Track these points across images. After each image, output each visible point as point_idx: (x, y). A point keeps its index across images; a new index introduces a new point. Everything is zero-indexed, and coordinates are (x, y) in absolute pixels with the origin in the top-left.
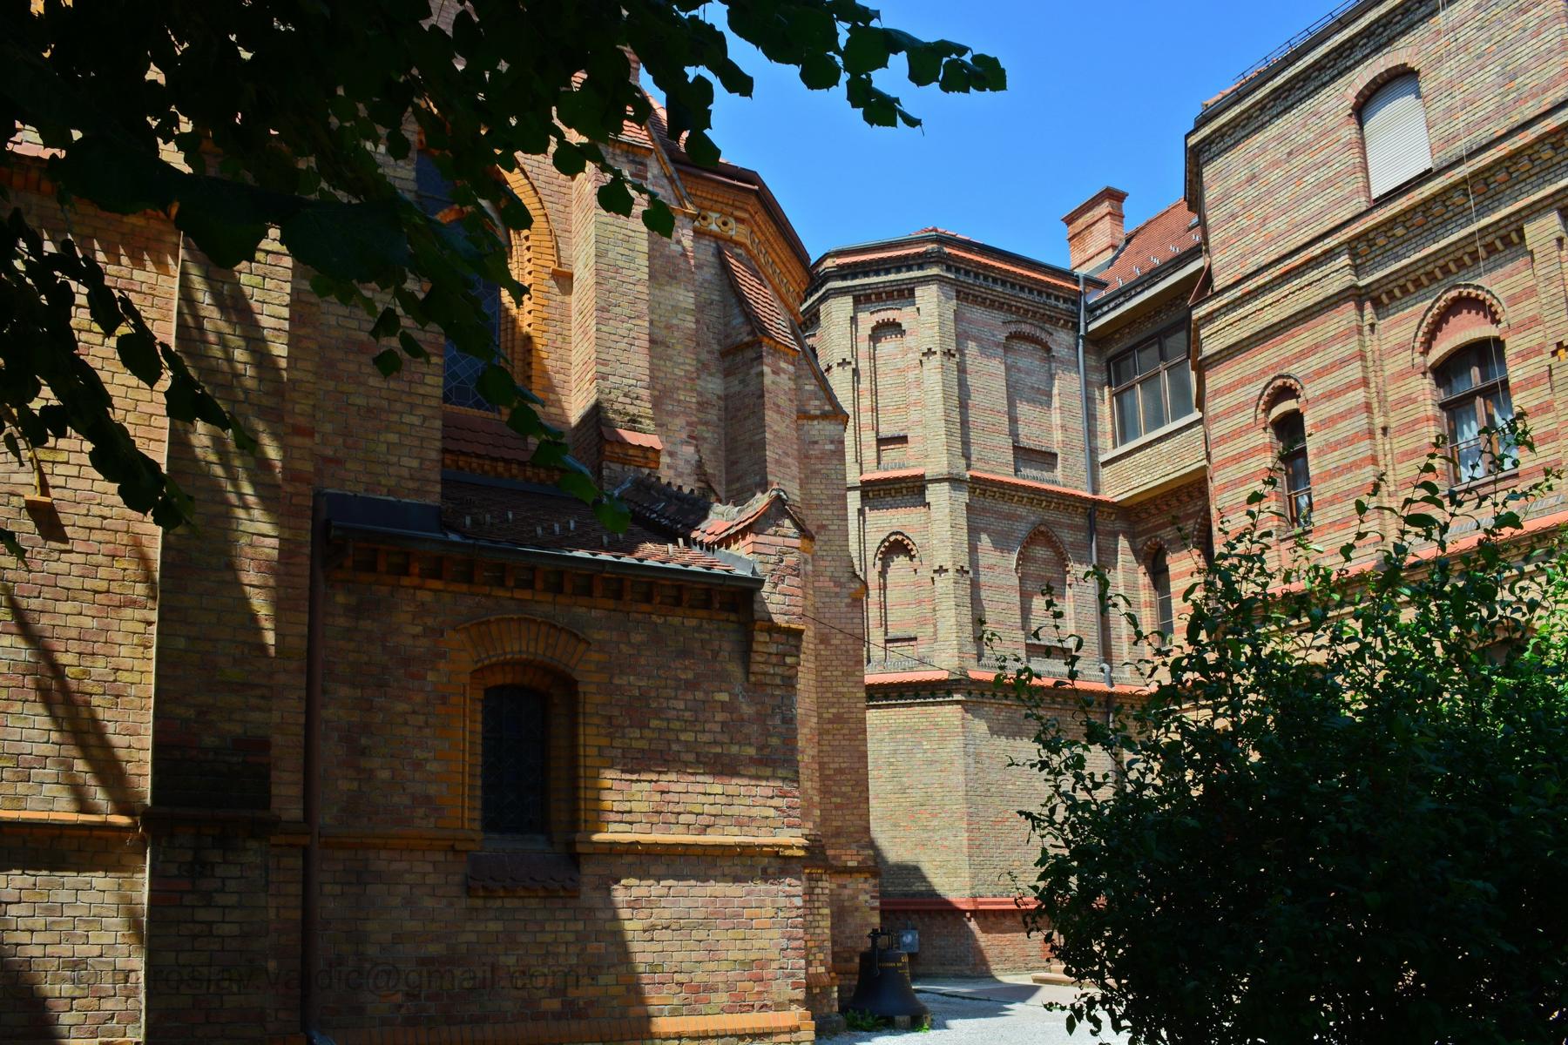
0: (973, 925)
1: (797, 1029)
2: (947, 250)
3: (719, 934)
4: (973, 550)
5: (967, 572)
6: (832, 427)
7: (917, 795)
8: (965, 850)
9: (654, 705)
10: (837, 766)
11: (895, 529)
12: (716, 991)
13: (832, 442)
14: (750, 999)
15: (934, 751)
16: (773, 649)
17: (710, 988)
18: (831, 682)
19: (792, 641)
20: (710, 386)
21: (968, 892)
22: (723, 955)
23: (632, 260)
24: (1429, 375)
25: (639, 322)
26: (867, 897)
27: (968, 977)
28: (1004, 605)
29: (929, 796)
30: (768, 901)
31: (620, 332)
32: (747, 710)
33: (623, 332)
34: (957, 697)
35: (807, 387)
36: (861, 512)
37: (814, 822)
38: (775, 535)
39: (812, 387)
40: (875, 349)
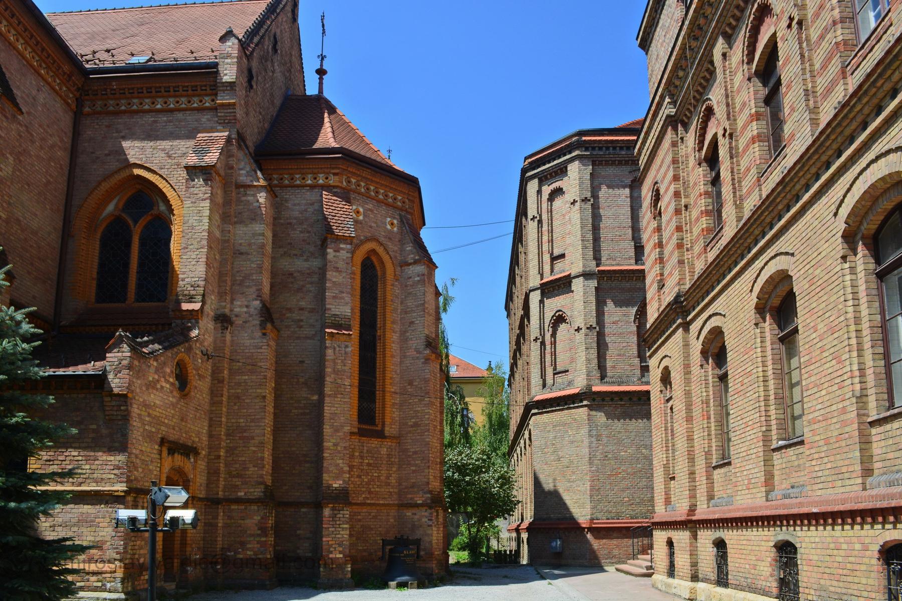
0: (589, 536)
1: (115, 572)
2: (584, 138)
3: (84, 530)
4: (600, 314)
5: (595, 328)
6: (418, 268)
7: (565, 461)
8: (588, 492)
10: (413, 450)
11: (559, 309)
13: (418, 276)
15: (574, 435)
16: (114, 403)
19: (122, 399)
21: (589, 517)
23: (201, 221)
24: (704, 164)
25: (202, 250)
26: (426, 520)
27: (586, 567)
28: (624, 344)
29: (571, 462)
30: (107, 515)
31: (192, 257)
32: (104, 431)
33: (194, 257)
34: (585, 403)
35: (408, 249)
36: (542, 302)
37: (344, 481)
38: (118, 352)
39: (410, 248)
40: (551, 205)
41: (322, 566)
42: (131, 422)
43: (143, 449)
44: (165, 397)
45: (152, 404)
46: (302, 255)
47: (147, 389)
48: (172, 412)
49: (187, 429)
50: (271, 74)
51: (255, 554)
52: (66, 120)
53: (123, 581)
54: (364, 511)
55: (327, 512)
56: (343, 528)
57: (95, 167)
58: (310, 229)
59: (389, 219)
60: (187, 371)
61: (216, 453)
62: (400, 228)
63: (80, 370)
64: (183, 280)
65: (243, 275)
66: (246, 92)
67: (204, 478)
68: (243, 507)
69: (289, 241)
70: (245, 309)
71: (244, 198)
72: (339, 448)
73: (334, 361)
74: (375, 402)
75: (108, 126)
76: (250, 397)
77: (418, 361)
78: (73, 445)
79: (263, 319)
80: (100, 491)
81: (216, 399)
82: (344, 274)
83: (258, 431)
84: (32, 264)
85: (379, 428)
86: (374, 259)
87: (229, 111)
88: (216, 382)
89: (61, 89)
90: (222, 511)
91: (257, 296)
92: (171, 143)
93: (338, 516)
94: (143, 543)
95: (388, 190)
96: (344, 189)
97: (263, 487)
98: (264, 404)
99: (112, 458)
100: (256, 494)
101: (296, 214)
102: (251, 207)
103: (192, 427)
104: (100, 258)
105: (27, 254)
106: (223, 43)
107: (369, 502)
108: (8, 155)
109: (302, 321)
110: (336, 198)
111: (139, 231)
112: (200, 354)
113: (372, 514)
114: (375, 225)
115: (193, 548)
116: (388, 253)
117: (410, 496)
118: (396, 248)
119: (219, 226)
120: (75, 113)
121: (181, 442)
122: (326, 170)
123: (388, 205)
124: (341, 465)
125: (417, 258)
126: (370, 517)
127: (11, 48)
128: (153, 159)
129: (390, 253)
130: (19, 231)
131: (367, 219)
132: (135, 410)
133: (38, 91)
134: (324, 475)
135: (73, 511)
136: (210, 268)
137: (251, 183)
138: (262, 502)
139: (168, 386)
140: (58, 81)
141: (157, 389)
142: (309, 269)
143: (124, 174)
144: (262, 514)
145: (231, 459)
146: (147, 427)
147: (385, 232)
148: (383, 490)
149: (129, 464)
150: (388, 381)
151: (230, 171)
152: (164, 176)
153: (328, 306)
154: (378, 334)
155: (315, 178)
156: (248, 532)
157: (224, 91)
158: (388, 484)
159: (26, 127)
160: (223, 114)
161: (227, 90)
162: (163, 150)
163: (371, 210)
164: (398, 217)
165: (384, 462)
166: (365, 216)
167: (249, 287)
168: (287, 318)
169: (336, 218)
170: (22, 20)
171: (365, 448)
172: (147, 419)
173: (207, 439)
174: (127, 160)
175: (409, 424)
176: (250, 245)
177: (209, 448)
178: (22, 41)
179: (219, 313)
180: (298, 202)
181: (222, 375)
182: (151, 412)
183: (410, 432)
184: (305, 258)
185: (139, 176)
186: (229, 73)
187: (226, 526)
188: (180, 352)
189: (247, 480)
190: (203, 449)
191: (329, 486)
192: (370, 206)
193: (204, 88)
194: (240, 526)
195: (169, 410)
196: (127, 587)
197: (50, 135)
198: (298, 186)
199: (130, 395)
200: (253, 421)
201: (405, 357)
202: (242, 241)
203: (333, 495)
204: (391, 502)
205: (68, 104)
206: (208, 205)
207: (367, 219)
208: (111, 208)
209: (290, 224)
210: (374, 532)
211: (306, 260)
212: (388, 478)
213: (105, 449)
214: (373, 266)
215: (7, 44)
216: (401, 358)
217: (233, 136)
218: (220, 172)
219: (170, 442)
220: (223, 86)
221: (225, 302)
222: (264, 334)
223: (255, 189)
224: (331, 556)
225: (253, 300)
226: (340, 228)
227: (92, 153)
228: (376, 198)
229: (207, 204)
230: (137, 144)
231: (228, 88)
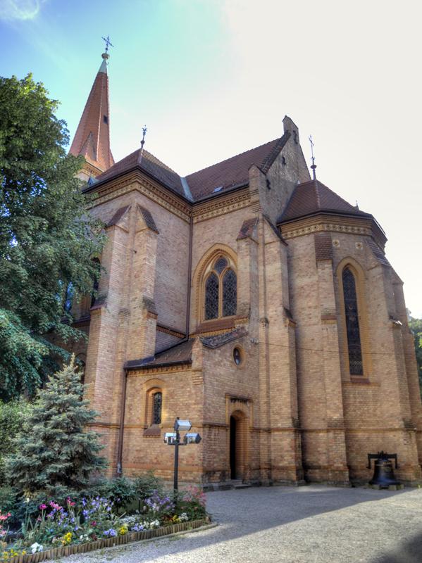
32: (193, 391)
51: (289, 464)
59: (356, 243)
64: (321, 279)
70: (275, 313)
101: (302, 252)
109: (310, 314)
116: (359, 264)
117: (390, 423)
139: (229, 363)
158: (375, 415)
163: (344, 240)
166: (341, 244)
200: (283, 379)
209: (299, 258)
212: (375, 411)
214: (351, 274)
224: (335, 465)
229: (248, 258)
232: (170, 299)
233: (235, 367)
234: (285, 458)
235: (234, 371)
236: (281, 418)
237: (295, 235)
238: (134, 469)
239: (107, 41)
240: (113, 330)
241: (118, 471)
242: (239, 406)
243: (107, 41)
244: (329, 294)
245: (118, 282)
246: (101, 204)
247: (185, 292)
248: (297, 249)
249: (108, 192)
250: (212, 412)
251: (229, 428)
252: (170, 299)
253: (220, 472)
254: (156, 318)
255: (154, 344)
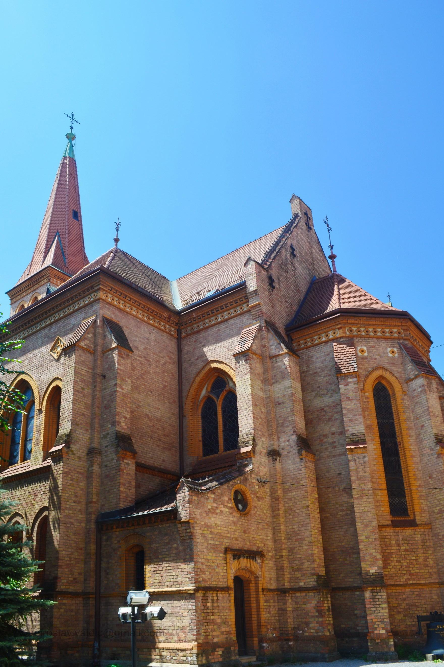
9: (159, 551)
12: (174, 636)
13: (420, 387)
14: (183, 639)
16: (183, 528)
17: (172, 635)
18: (435, 495)
19: (187, 525)
20: (337, 397)
22: (175, 624)
25: (250, 408)
31: (245, 415)
32: (181, 548)
35: (409, 368)
37: (378, 567)
41: (369, 641)
42: (195, 540)
43: (209, 558)
44: (226, 518)
45: (214, 525)
46: (327, 394)
47: (208, 514)
48: (234, 528)
49: (251, 538)
50: (293, 272)
51: (316, 632)
52: (172, 345)
53: (197, 656)
54: (407, 590)
55: (368, 594)
56: (382, 608)
57: (192, 369)
58: (329, 373)
59: (389, 349)
60: (246, 496)
61: (280, 554)
62: (401, 353)
63: (164, 509)
65: (282, 419)
66: (269, 292)
67: (273, 574)
68: (304, 594)
69: (318, 385)
70: (287, 443)
71: (276, 365)
72: (371, 540)
73: (356, 470)
74: (405, 497)
75: (195, 341)
76: (299, 508)
77: (432, 457)
78: (166, 559)
79: (299, 448)
80: (181, 590)
81: (275, 513)
82: (355, 402)
83: (306, 534)
84: (160, 440)
85: (412, 518)
86: (384, 382)
87: (257, 309)
88: (274, 500)
89: (165, 327)
90: (289, 598)
91: (294, 432)
92: (229, 341)
93: (377, 597)
94: (215, 627)
95: (383, 327)
96: (348, 337)
97: (315, 577)
98: (308, 512)
99: (186, 566)
100: (311, 583)
101: (319, 365)
102: (281, 370)
103: (255, 536)
104: (203, 427)
105: (156, 435)
106: (246, 267)
107: (411, 582)
108: (127, 379)
109: (335, 442)
110: (342, 346)
111: (221, 403)
112: (257, 482)
113: (416, 593)
114: (379, 357)
115: (268, 629)
116: (393, 375)
118: (400, 370)
119: (261, 388)
120: (178, 339)
121: (245, 549)
122: (332, 328)
123: (386, 339)
124: (374, 554)
125: (416, 373)
126: (413, 596)
127: (129, 315)
128: (221, 354)
129: (396, 375)
130: (148, 422)
131: (371, 354)
132: (197, 531)
133: (150, 333)
134: (362, 563)
135: (169, 605)
136: (258, 419)
137: (279, 353)
138: (316, 590)
140: (163, 324)
141: (217, 514)
142: (333, 402)
143: (207, 369)
144: (317, 599)
145: (291, 557)
146: (210, 542)
147: (388, 360)
148: (422, 571)
149: (196, 570)
150: (412, 478)
151: (264, 349)
152: (228, 364)
153: (346, 429)
154: (398, 441)
155: (327, 336)
156: (310, 614)
157: (252, 297)
158: (426, 566)
159: (145, 357)
160: (254, 313)
161: (253, 296)
162: (225, 347)
163: (373, 347)
164: (397, 345)
165: (420, 547)
166: (369, 352)
167: (287, 426)
168: (325, 443)
169: (344, 360)
170: (131, 297)
171: (400, 537)
172: (210, 536)
173: (272, 543)
174: (207, 359)
175: (436, 511)
176: (284, 396)
177: (276, 550)
178: (135, 309)
179: (270, 449)
180: (319, 356)
181: (277, 494)
182: (213, 530)
183: (437, 518)
184: (330, 395)
185: (215, 368)
186: (252, 286)
187: (295, 610)
188: (237, 484)
189: (304, 572)
190: (269, 551)
191: (367, 573)
192: (372, 344)
193: (241, 300)
194: (304, 610)
195: (230, 527)
196: (201, 661)
197: (162, 357)
198: (317, 345)
199: (190, 521)
200: (302, 526)
201: (423, 455)
202: (280, 395)
203: (371, 579)
204: (432, 581)
205: (172, 335)
206: (249, 376)
207: (371, 354)
208: (204, 392)
209: (316, 373)
210: (419, 609)
211: (331, 397)
212: (425, 560)
213: (182, 561)
215: (126, 313)
216: (420, 457)
217: (263, 325)
218: (257, 352)
219: (232, 550)
220: (251, 295)
221: (273, 440)
222: (302, 459)
223: (282, 356)
224: (376, 632)
225: (291, 435)
226: (346, 367)
227: (190, 360)
228: (375, 336)
229: (248, 376)
230: (212, 347)
231: (254, 295)
232: (155, 433)
233: (236, 514)
234: (311, 625)
235: (235, 519)
236: (303, 575)
237: (309, 344)
238: (115, 649)
239: (72, 117)
240: (80, 476)
241: (96, 652)
242: (244, 562)
243: (72, 117)
244: (355, 415)
245: (83, 415)
246: (60, 319)
247: (177, 424)
248: (313, 362)
249: (67, 304)
250: (207, 573)
251: (232, 593)
252: (155, 433)
253: (222, 649)
254: (134, 458)
255: (133, 490)
